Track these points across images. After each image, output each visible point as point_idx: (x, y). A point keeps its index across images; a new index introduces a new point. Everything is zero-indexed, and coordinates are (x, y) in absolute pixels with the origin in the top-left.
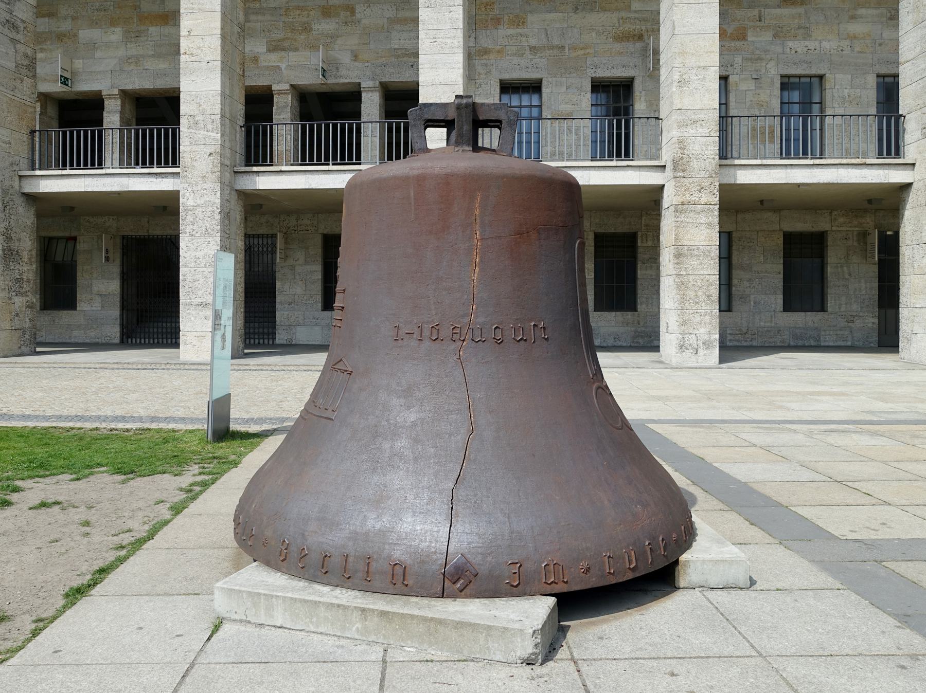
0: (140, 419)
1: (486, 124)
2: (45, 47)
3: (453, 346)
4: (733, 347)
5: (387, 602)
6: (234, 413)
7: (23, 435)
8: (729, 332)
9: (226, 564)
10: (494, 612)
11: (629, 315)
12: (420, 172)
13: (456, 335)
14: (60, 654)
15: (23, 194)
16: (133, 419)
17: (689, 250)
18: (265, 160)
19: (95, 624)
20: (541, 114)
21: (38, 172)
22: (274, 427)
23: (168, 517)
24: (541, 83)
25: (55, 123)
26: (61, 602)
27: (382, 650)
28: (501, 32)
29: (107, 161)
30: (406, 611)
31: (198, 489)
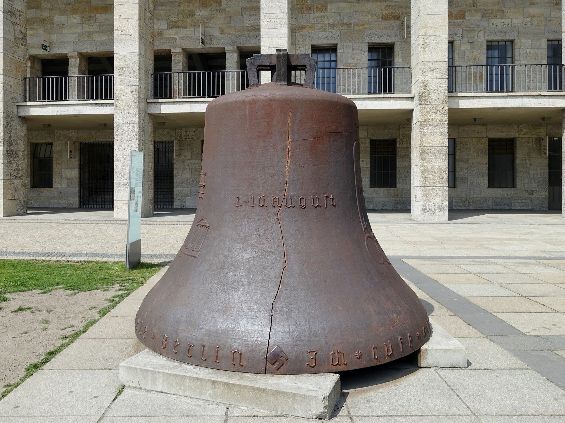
0: (87, 255)
1: (296, 68)
2: (33, 27)
3: (274, 210)
4: (458, 209)
5: (229, 377)
6: (143, 251)
7: (13, 264)
8: (454, 200)
9: (131, 349)
10: (299, 384)
11: (392, 190)
12: (253, 98)
13: (276, 203)
14: (18, 409)
15: (19, 117)
16: (82, 255)
17: (429, 149)
18: (166, 95)
19: (43, 389)
20: (336, 66)
21: (29, 103)
22: (169, 260)
23: (97, 318)
24: (337, 47)
25: (40, 73)
26: (24, 373)
27: (225, 408)
28: (312, 15)
29: (70, 97)
30: (241, 383)
31: (117, 299)
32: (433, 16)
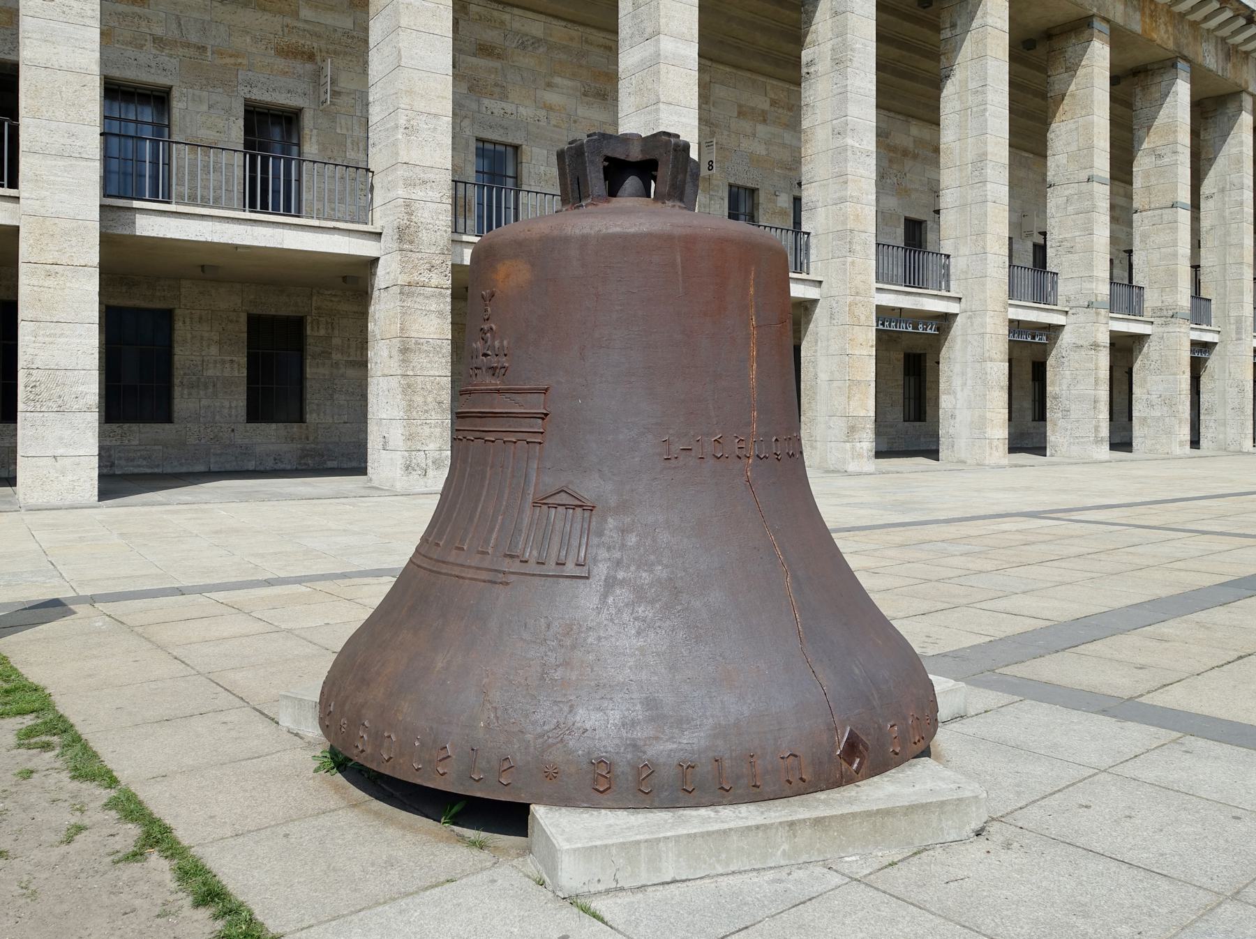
11: (295, 428)
17: (417, 343)
32: (425, 75)
